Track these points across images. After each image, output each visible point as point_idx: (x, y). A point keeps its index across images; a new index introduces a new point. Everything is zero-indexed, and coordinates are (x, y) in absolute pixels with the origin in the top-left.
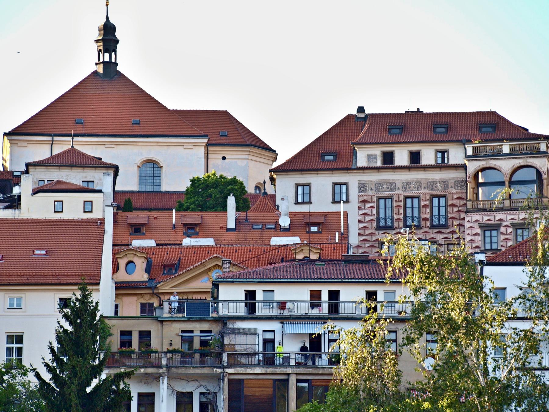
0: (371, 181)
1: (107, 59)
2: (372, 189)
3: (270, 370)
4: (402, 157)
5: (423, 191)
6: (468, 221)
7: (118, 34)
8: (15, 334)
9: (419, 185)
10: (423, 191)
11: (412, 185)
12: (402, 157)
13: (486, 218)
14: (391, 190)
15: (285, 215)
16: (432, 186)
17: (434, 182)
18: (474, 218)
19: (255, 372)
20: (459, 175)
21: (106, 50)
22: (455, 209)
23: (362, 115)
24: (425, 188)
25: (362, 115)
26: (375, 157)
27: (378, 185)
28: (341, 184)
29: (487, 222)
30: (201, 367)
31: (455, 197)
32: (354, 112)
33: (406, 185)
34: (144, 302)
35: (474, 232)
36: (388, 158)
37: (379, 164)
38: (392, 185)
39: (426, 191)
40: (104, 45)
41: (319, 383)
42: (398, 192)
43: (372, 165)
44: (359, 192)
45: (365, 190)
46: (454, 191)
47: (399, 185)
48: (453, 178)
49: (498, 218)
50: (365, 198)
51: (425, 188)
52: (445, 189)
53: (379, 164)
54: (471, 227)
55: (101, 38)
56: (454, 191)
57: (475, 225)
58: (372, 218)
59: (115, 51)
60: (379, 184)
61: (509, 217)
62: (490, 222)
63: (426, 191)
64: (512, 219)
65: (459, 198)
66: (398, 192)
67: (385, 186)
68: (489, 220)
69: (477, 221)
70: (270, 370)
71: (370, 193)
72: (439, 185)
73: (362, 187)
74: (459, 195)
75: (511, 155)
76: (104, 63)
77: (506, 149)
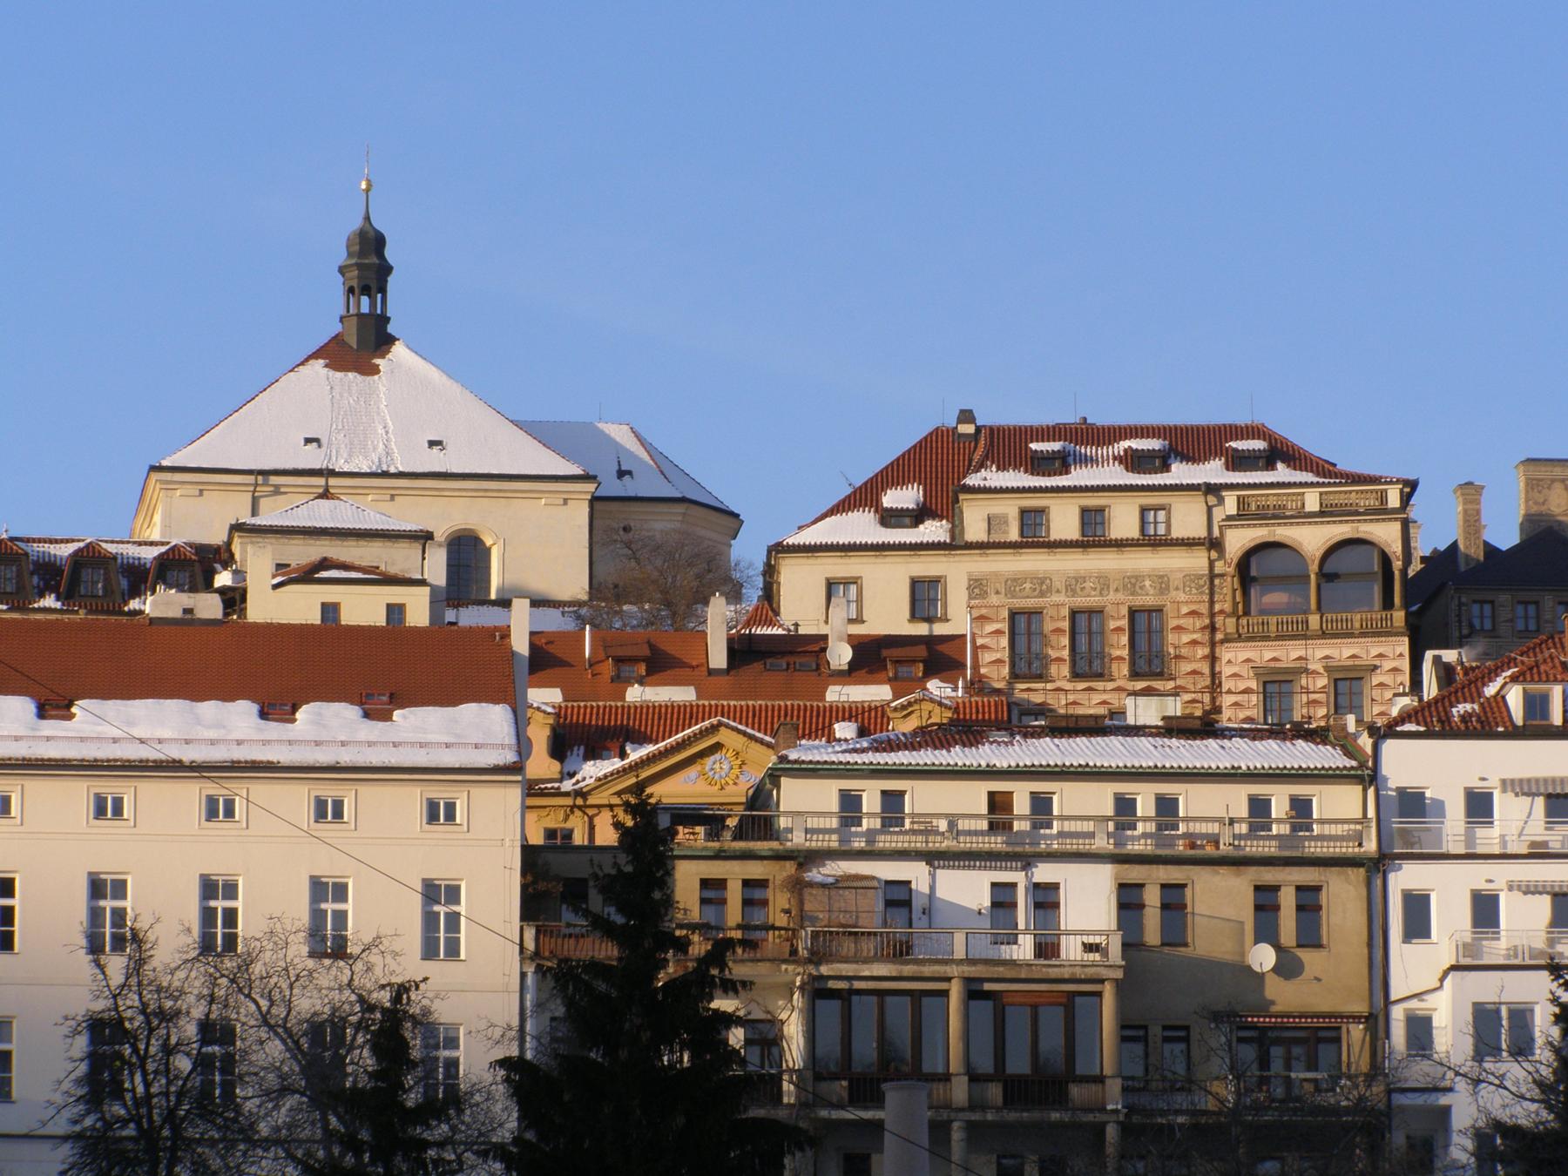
0: (996, 574)
1: (365, 308)
2: (997, 593)
3: (908, 970)
4: (1064, 521)
5: (1112, 596)
6: (1229, 661)
7: (389, 254)
8: (331, 881)
9: (1103, 582)
10: (1112, 596)
11: (1089, 584)
12: (1064, 521)
13: (1268, 655)
14: (1042, 594)
15: (841, 640)
16: (1134, 585)
17: (1136, 577)
18: (1243, 656)
19: (875, 974)
20: (1198, 561)
21: (366, 290)
22: (1186, 638)
23: (968, 429)
24: (1117, 590)
25: (968, 429)
26: (1003, 520)
27: (1013, 583)
28: (1157, 509)
29: (1272, 664)
30: (752, 961)
31: (1185, 610)
32: (951, 422)
33: (1075, 583)
34: (552, 825)
35: (1242, 686)
36: (1032, 520)
37: (1014, 535)
38: (1042, 584)
39: (1120, 596)
40: (359, 278)
41: (1017, 999)
42: (1056, 598)
43: (997, 537)
44: (970, 598)
45: (984, 595)
46: (1182, 597)
47: (1057, 584)
48: (1181, 570)
49: (1294, 655)
50: (984, 611)
51: (1117, 590)
52: (1162, 593)
53: (1014, 535)
54: (1235, 675)
55: (353, 261)
56: (1182, 597)
57: (1244, 670)
58: (998, 656)
59: (383, 290)
60: (1015, 580)
61: (1320, 654)
62: (1278, 665)
63: (1120, 596)
64: (1327, 657)
65: (1193, 613)
66: (1056, 598)
67: (1028, 585)
68: (1275, 659)
69: (1248, 660)
70: (908, 970)
71: (994, 599)
72: (1147, 583)
73: (977, 587)
74: (1193, 607)
75: (1326, 513)
76: (360, 316)
77: (1312, 501)
